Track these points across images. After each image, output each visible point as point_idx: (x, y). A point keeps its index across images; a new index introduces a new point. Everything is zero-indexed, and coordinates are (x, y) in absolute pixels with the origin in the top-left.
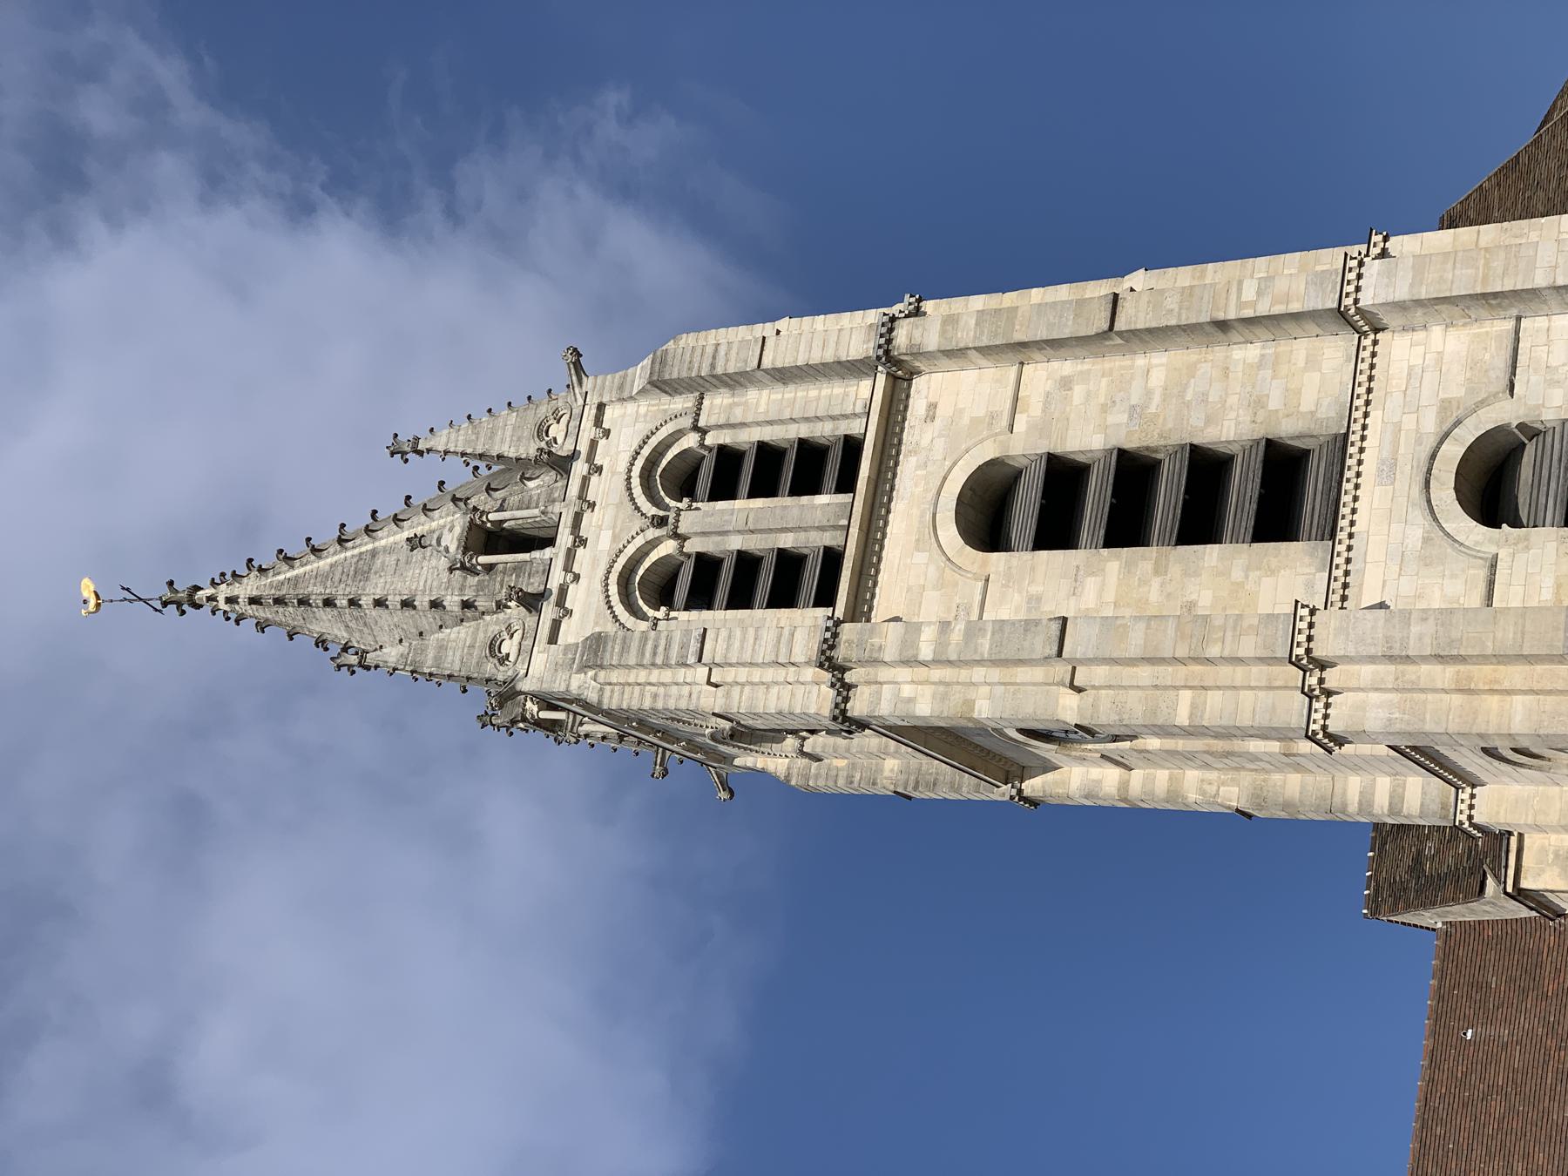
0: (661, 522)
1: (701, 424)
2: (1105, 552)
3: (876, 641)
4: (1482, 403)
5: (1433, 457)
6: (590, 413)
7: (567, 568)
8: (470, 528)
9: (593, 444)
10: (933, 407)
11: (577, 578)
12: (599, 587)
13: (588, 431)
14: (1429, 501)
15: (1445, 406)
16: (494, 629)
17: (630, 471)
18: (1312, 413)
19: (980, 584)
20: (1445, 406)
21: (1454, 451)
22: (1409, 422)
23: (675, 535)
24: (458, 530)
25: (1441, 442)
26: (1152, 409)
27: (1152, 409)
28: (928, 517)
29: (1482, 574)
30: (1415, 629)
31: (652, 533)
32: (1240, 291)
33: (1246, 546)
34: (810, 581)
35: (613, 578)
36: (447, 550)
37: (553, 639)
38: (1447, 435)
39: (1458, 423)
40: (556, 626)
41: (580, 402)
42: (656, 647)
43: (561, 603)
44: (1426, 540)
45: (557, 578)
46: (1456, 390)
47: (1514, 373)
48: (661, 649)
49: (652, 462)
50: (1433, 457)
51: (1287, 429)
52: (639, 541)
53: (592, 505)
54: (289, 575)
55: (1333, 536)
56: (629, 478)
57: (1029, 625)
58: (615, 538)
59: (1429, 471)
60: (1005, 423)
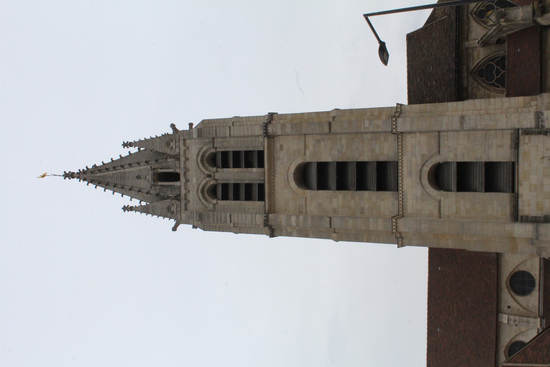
0: (209, 176)
1: (215, 146)
2: (337, 192)
3: (279, 220)
4: (432, 156)
5: (421, 171)
6: (181, 142)
7: (186, 189)
8: (154, 175)
9: (185, 151)
10: (281, 146)
11: (189, 191)
12: (196, 194)
13: (182, 148)
14: (421, 183)
15: (423, 156)
16: (168, 204)
17: (197, 160)
18: (388, 155)
19: (304, 200)
20: (423, 156)
21: (426, 169)
22: (414, 160)
23: (214, 179)
24: (150, 175)
25: (423, 167)
26: (344, 151)
27: (344, 151)
28: (286, 179)
29: (437, 204)
30: (423, 226)
31: (208, 179)
32: (364, 123)
33: (375, 192)
34: (255, 191)
35: (199, 191)
36: (149, 180)
37: (186, 209)
38: (424, 164)
39: (426, 161)
40: (186, 205)
41: (178, 137)
42: (217, 218)
43: (186, 199)
44: (422, 194)
45: (183, 191)
46: (425, 152)
47: (439, 148)
48: (219, 218)
49: (203, 156)
50: (421, 171)
51: (382, 159)
52: (204, 181)
53: (188, 170)
54: (98, 175)
55: (398, 190)
56: (197, 162)
57: (321, 217)
58: (197, 179)
59: (421, 175)
60: (303, 152)
